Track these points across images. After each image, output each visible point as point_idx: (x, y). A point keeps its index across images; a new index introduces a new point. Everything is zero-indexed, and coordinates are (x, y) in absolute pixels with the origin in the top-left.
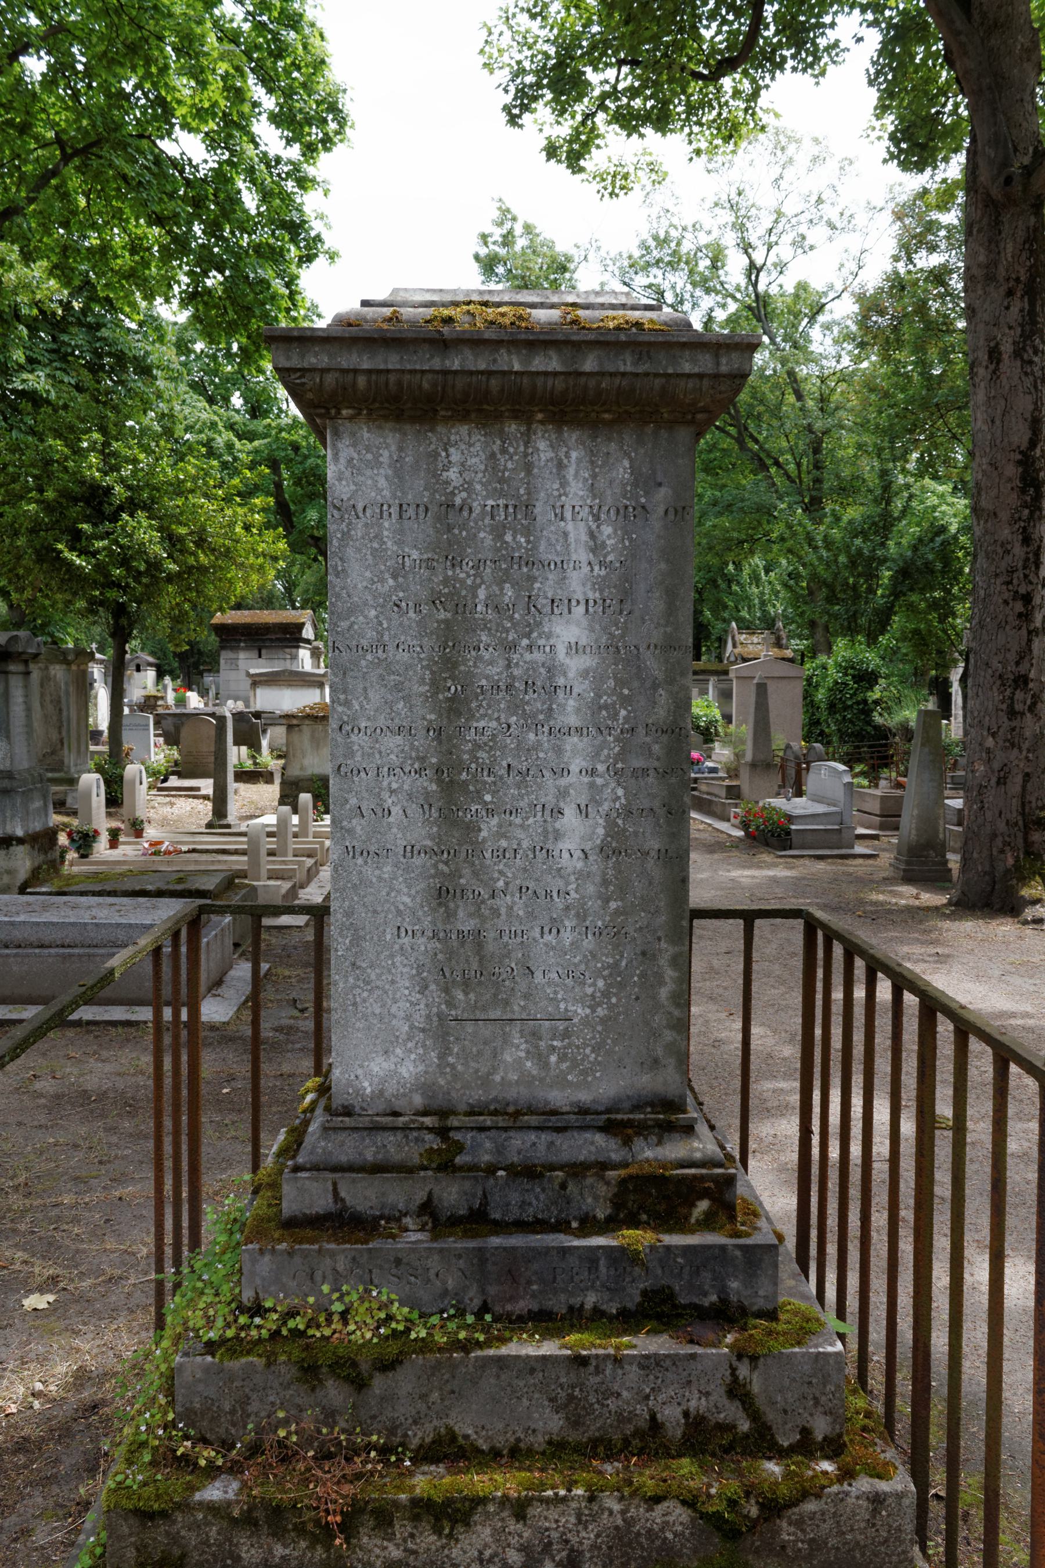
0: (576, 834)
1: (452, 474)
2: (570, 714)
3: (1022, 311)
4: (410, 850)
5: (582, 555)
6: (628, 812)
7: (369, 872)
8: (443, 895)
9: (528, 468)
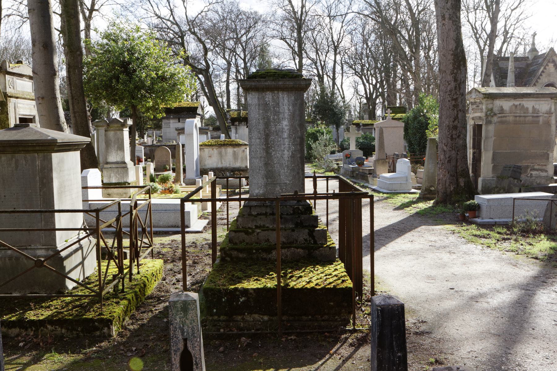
1: (267, 99)
2: (286, 135)
3: (452, 4)
4: (261, 157)
5: (287, 111)
6: (295, 151)
7: (255, 161)
8: (266, 164)
9: (278, 98)
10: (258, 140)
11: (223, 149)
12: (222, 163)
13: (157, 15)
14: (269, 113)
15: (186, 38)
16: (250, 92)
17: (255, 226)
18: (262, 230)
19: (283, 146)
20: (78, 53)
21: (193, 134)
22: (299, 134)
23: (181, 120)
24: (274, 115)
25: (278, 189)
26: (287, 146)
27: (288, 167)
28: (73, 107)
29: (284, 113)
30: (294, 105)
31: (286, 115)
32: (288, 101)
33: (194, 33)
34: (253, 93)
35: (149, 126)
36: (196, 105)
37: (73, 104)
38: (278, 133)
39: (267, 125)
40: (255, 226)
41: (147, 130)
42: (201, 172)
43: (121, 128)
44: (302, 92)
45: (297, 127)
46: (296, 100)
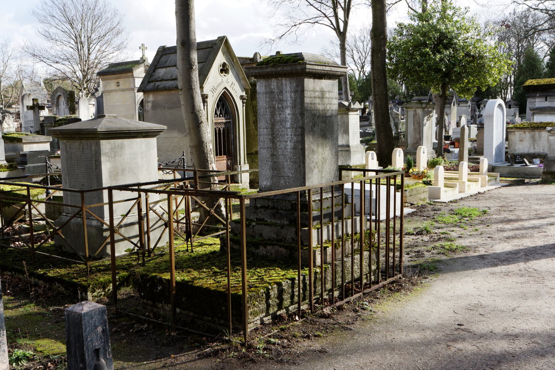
0: (290, 145)
1: (272, 87)
2: (288, 125)
4: (268, 148)
5: (289, 99)
8: (273, 155)
9: (282, 85)
10: (265, 130)
11: (537, 133)
12: (534, 148)
17: (256, 218)
18: (257, 224)
20: (382, 37)
21: (493, 116)
23: (548, 98)
24: (279, 104)
28: (374, 90)
29: (286, 101)
31: (289, 104)
32: (291, 88)
37: (374, 87)
39: (273, 114)
40: (256, 218)
43: (347, 112)
44: (302, 77)
45: (299, 116)
46: (297, 86)
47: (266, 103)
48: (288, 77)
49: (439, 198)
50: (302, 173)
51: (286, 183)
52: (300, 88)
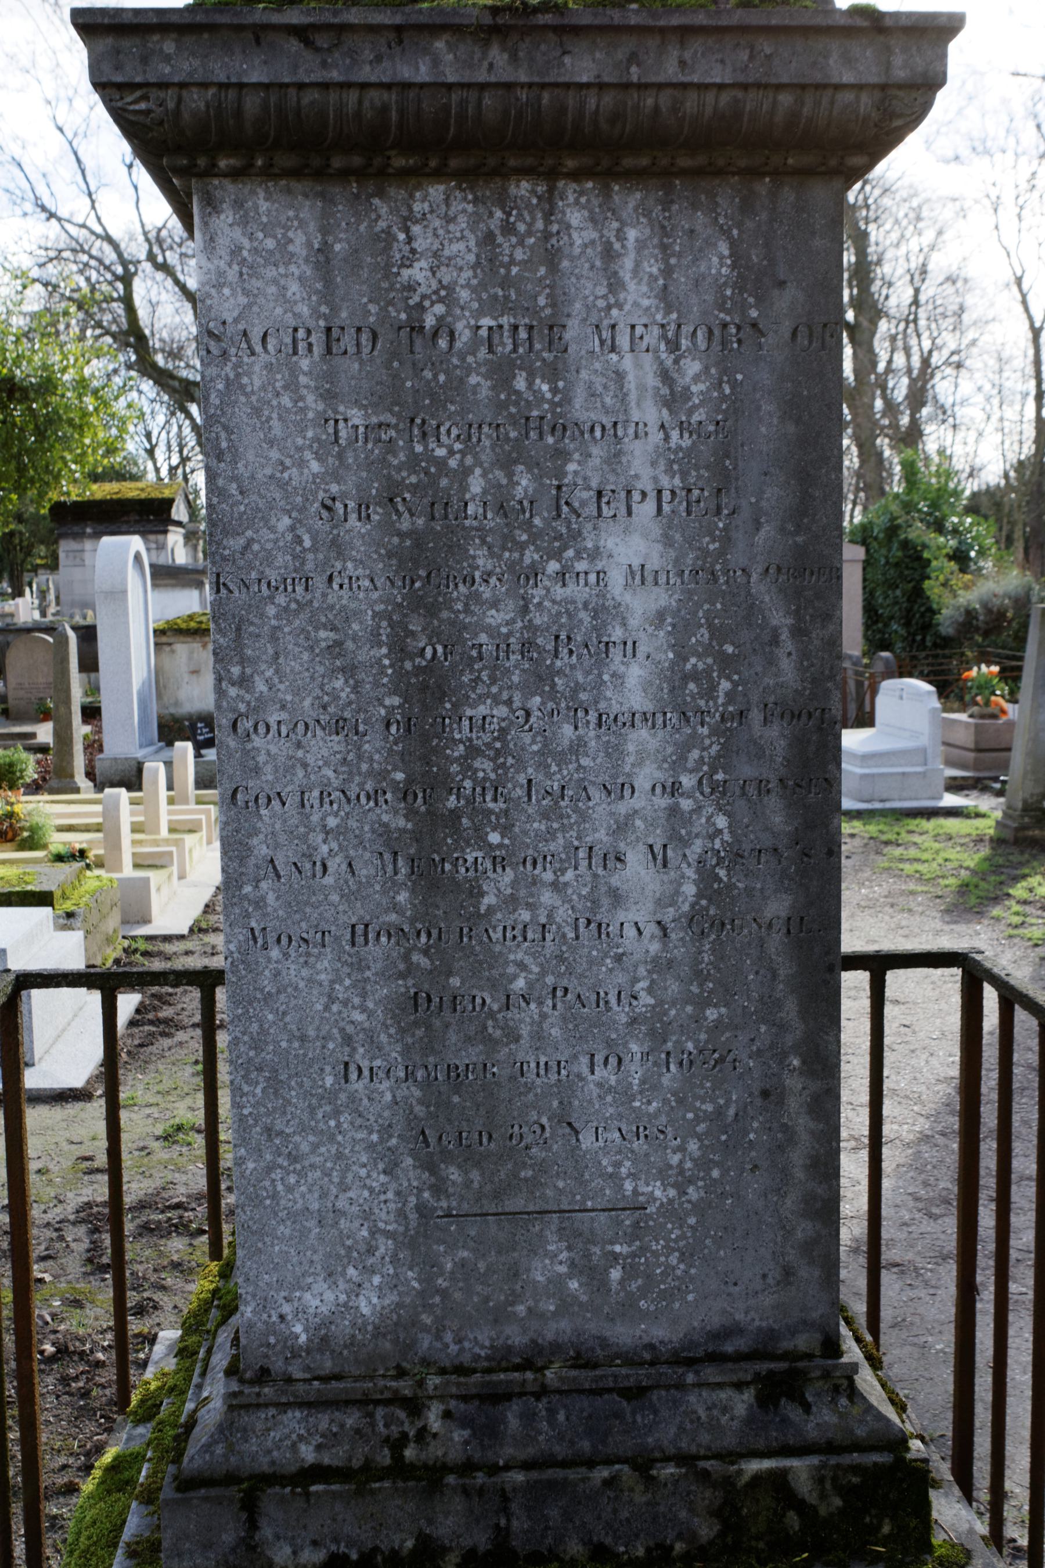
0: (646, 893)
1: (418, 272)
2: (633, 684)
5: (650, 414)
6: (735, 856)
7: (293, 972)
8: (422, 1009)
9: (552, 258)
10: (323, 747)
13: (43, 208)
14: (450, 435)
15: (140, 289)
16: (227, 190)
19: (599, 806)
21: (125, 592)
22: (787, 667)
25: (550, 1264)
26: (644, 801)
27: (656, 1029)
29: (613, 432)
30: (732, 340)
31: (641, 462)
33: (164, 268)
34: (263, 203)
35: (39, 561)
36: (167, 493)
38: (558, 659)
39: (426, 564)
41: (35, 569)
42: (161, 726)
46: (753, 279)
47: (330, 446)
48: (634, 176)
49: (146, 921)
50: (797, 1157)
51: (593, 1275)
52: (787, 302)
